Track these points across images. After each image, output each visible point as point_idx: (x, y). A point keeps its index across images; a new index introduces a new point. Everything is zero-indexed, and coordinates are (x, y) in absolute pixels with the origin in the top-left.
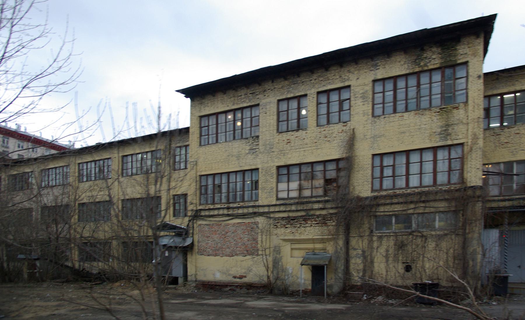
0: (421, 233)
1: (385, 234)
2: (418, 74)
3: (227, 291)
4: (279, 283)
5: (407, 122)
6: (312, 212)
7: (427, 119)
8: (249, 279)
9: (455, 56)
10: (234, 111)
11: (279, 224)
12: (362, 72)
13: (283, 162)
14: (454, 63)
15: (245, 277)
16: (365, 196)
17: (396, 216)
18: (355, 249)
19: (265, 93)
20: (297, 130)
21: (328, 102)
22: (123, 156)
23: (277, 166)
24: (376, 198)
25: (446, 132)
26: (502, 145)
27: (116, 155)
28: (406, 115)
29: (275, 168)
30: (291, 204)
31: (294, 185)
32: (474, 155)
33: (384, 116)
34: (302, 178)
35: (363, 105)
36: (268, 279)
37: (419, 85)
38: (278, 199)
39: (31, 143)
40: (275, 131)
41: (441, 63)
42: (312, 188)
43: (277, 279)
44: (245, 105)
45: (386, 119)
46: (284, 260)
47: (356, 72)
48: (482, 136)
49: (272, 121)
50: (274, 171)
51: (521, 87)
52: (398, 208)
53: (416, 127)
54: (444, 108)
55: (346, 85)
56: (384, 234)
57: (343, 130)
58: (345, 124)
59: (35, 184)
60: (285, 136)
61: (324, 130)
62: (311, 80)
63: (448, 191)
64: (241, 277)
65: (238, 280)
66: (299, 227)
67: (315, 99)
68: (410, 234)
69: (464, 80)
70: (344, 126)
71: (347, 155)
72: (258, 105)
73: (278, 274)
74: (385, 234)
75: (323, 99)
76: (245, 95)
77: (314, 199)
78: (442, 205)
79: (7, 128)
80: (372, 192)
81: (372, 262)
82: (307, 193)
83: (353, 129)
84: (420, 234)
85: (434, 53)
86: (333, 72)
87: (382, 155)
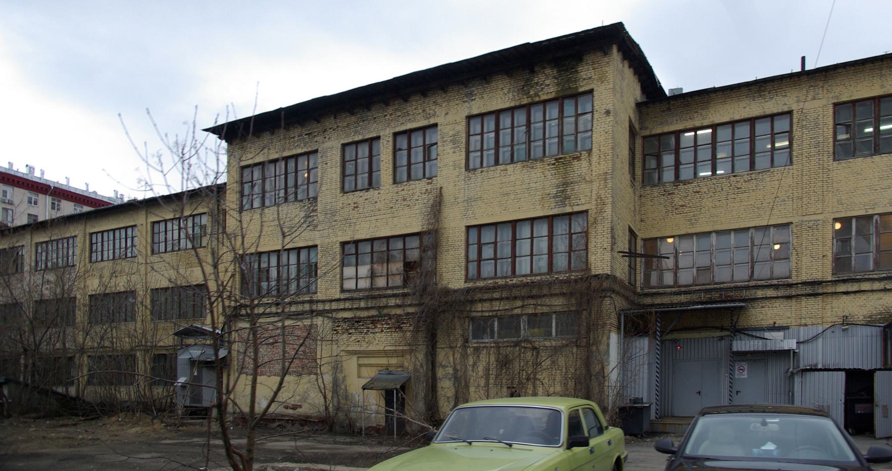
0: (531, 344)
1: (484, 345)
2: (528, 107)
3: (274, 429)
4: (341, 415)
5: (512, 178)
6: (385, 311)
7: (539, 175)
8: (304, 410)
9: (576, 81)
10: (286, 159)
11: (340, 328)
12: (452, 103)
13: (349, 237)
14: (574, 92)
15: (300, 406)
16: (456, 288)
17: (500, 318)
18: (444, 367)
19: (326, 133)
20: (367, 190)
21: (409, 148)
22: (154, 223)
23: (341, 242)
24: (468, 291)
25: (563, 194)
26: (676, 209)
27: (142, 220)
28: (510, 168)
29: (338, 245)
30: (360, 299)
31: (364, 270)
32: (600, 228)
33: (481, 170)
34: (375, 259)
35: (454, 152)
36: (326, 411)
37: (529, 124)
38: (343, 291)
39: (50, 195)
40: (338, 191)
41: (557, 92)
42: (388, 275)
43: (338, 409)
44: (299, 151)
45: (483, 174)
46: (348, 382)
47: (444, 105)
48: (611, 200)
49: (334, 176)
50: (337, 249)
51: (702, 122)
52: (497, 306)
53: (524, 186)
54: (561, 158)
55: (431, 123)
56: (481, 345)
57: (427, 190)
58: (430, 181)
59: (321, 217)
60: (351, 198)
61: (403, 190)
62: (386, 115)
63: (567, 282)
64: (295, 407)
65: (290, 411)
66: (366, 333)
67: (391, 143)
68: (517, 344)
69: (589, 116)
70: (428, 183)
71: (430, 227)
72: (316, 151)
73: (339, 402)
74: (484, 345)
75: (403, 142)
76: (299, 136)
77: (389, 292)
78: (558, 303)
79: (13, 173)
80: (465, 282)
81: (467, 386)
82: (381, 282)
83: (441, 188)
84: (530, 346)
85: (547, 77)
86: (414, 103)
87: (480, 227)
